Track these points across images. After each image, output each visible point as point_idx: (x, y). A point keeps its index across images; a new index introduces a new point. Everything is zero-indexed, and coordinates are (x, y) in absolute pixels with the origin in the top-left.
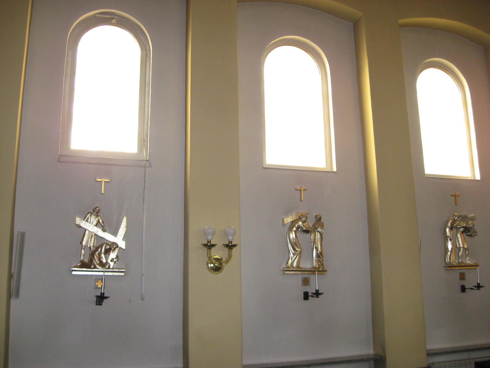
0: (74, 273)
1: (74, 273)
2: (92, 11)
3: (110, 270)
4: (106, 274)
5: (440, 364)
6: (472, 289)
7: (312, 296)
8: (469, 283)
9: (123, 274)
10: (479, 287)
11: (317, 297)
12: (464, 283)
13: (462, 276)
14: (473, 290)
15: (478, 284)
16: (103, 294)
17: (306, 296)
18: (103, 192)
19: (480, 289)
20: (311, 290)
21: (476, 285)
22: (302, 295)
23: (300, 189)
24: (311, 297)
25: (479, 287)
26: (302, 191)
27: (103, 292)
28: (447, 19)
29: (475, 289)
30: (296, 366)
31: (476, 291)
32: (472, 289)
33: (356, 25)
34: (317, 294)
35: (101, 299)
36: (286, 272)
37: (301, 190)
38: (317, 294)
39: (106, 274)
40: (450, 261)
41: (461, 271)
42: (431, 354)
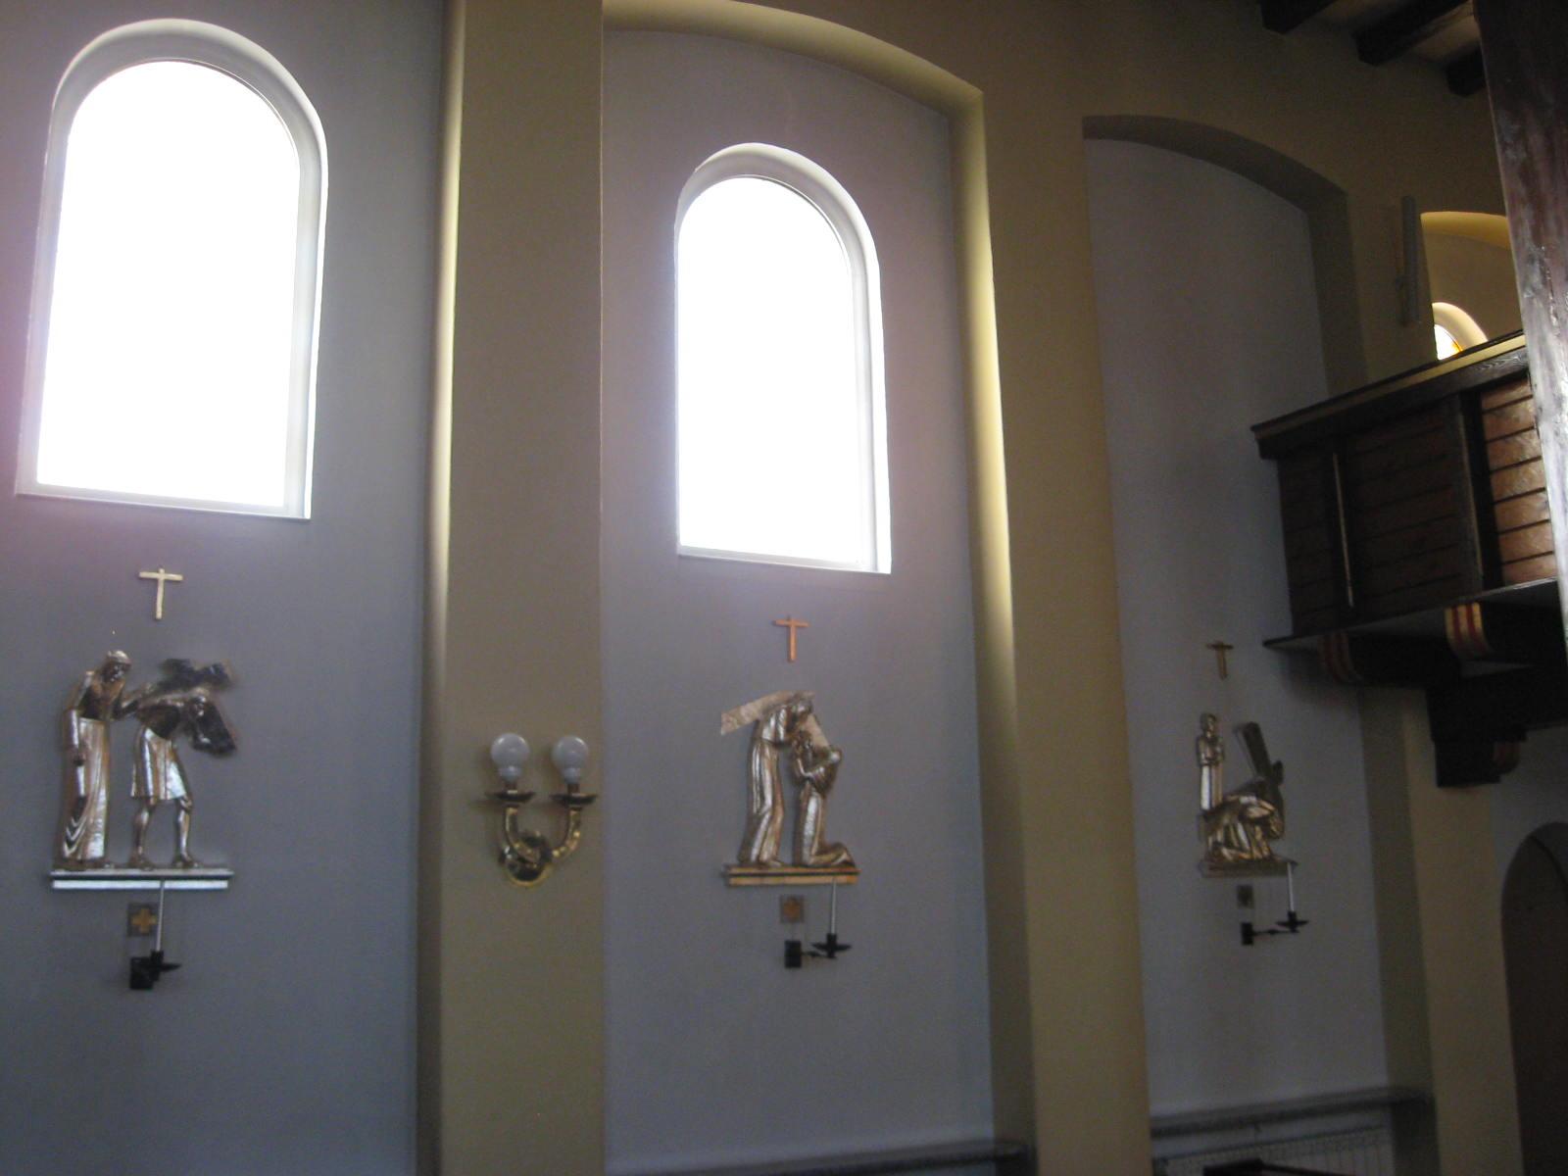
0: (59, 885)
1: (59, 885)
2: (1442, 211)
3: (830, 870)
4: (168, 885)
5: (1272, 1147)
6: (1272, 932)
7: (814, 955)
8: (1264, 917)
9: (223, 884)
10: (1293, 923)
11: (831, 956)
12: (1247, 915)
13: (1245, 896)
14: (1277, 936)
15: (1292, 915)
16: (157, 957)
17: (794, 956)
18: (159, 615)
19: (1299, 928)
20: (810, 935)
21: (1285, 918)
22: (780, 951)
23: (786, 623)
24: (810, 957)
25: (1293, 923)
26: (793, 630)
27: (836, 929)
28: (950, 69)
29: (1283, 932)
30: (900, 1167)
31: (1288, 941)
32: (1272, 932)
33: (948, 118)
34: (832, 947)
35: (147, 972)
36: (733, 881)
37: (788, 627)
38: (832, 947)
39: (168, 885)
40: (1268, 847)
41: (1244, 881)
42: (1162, 1131)
